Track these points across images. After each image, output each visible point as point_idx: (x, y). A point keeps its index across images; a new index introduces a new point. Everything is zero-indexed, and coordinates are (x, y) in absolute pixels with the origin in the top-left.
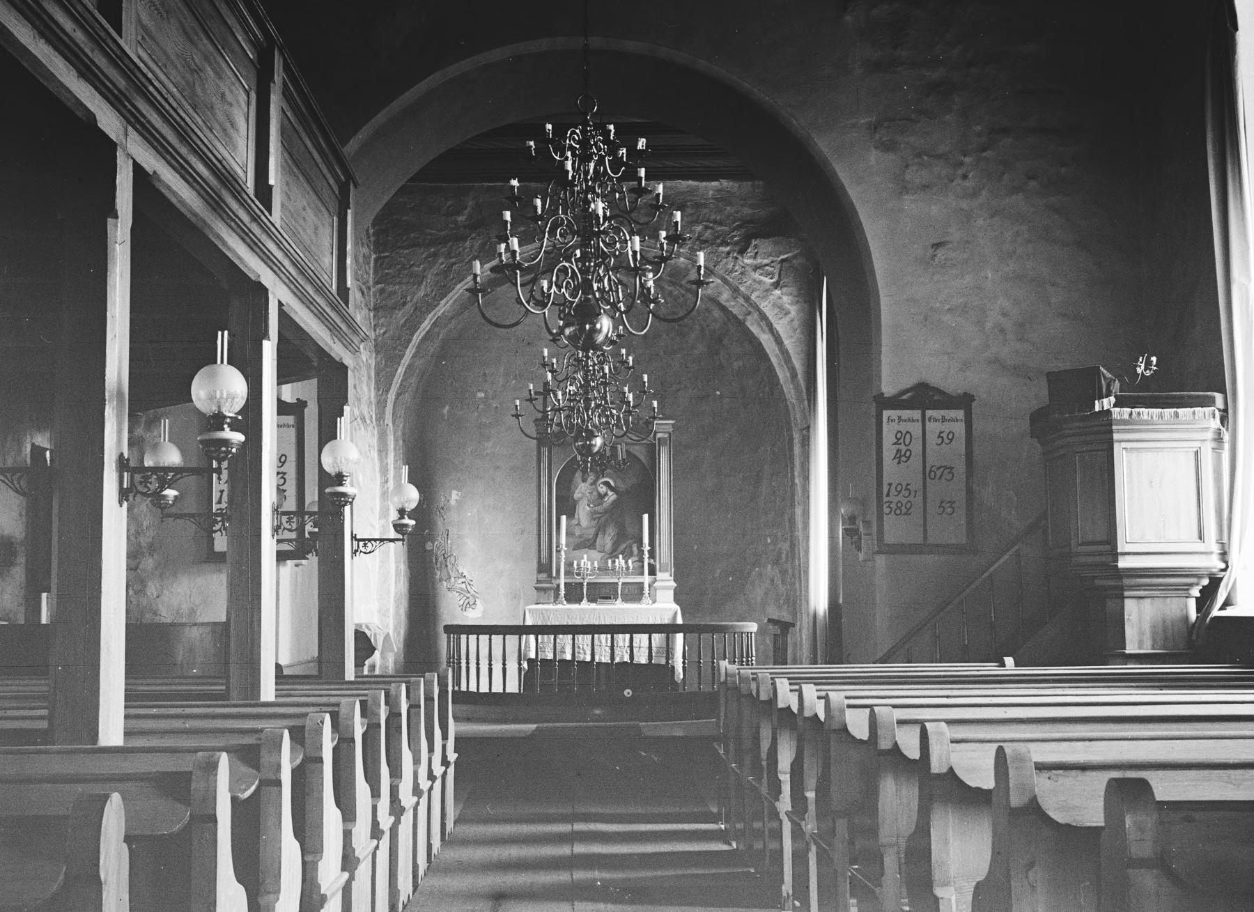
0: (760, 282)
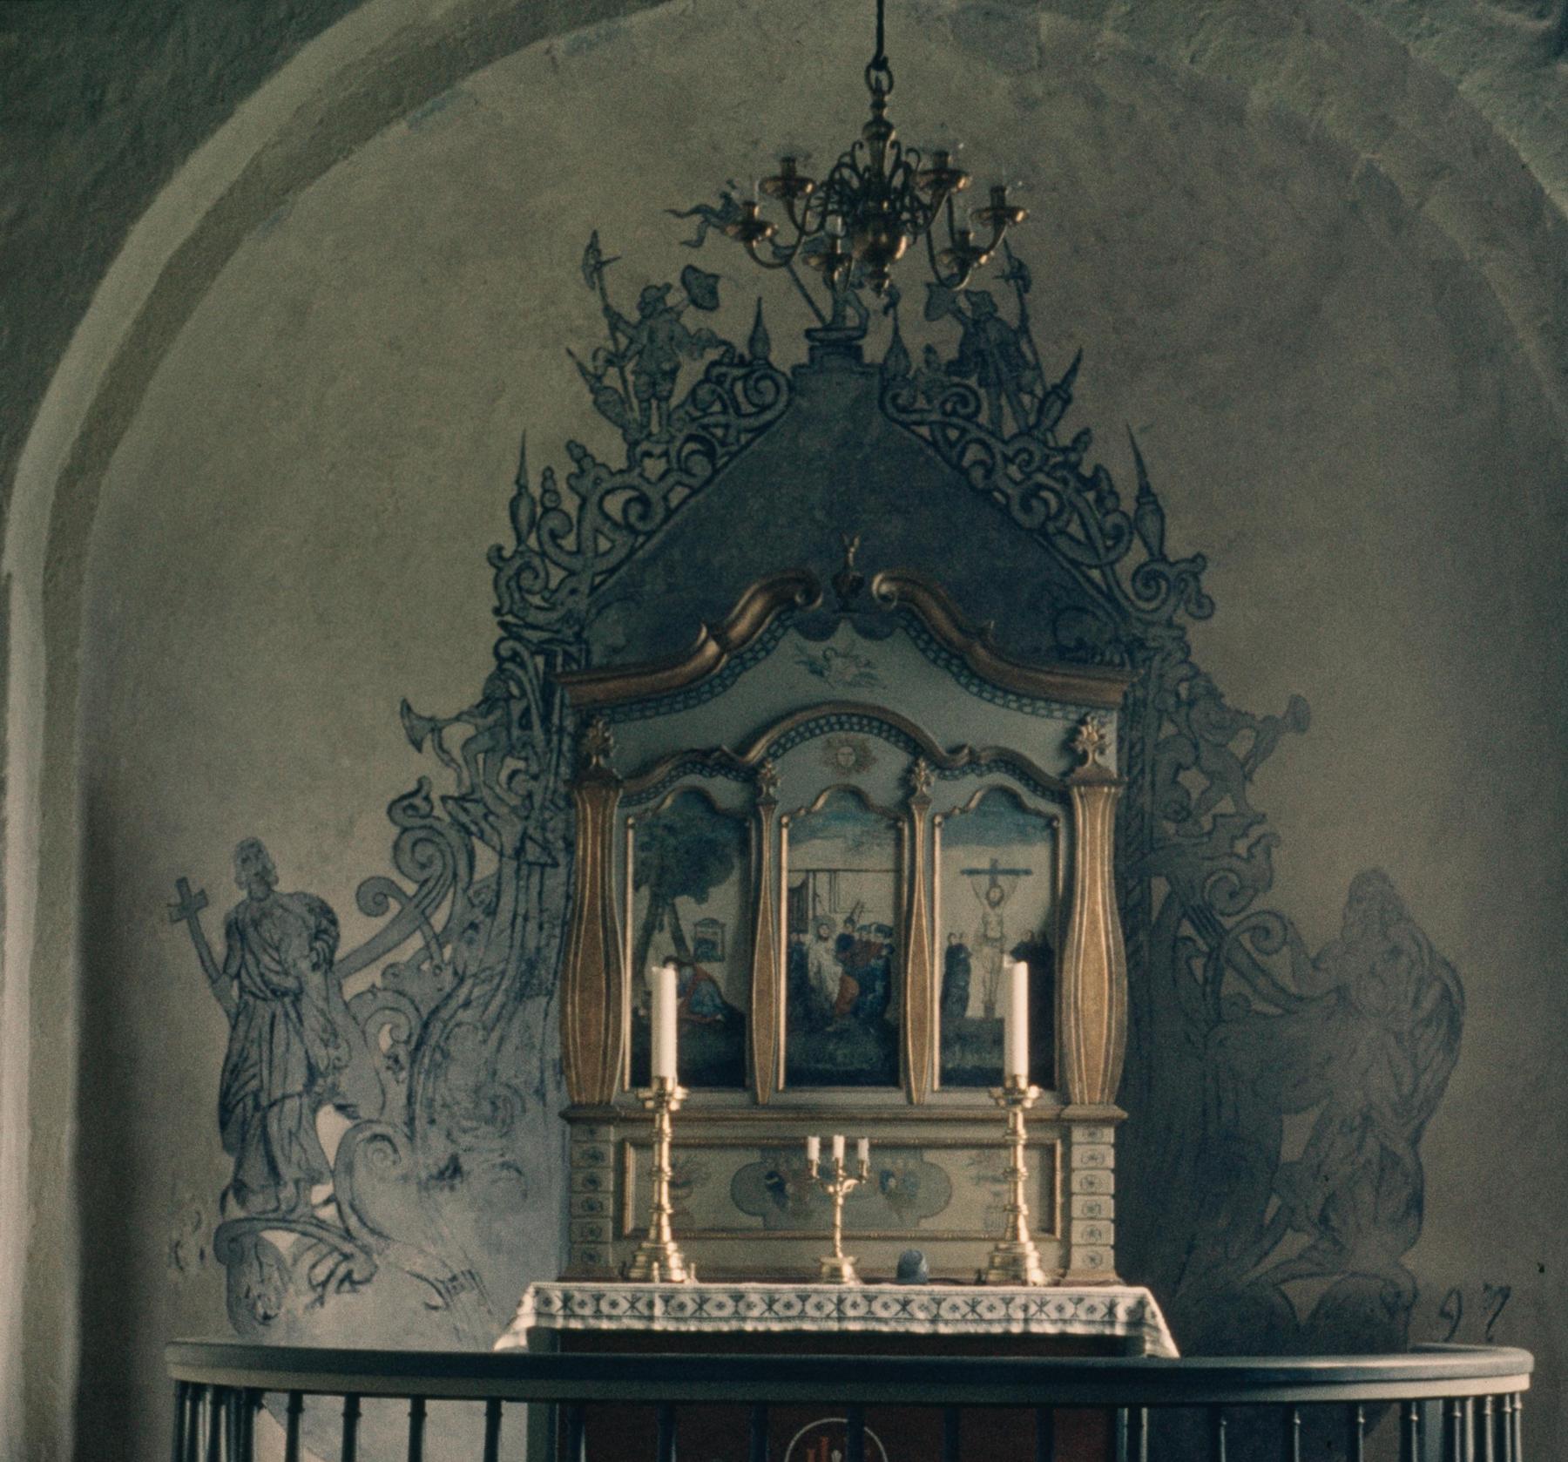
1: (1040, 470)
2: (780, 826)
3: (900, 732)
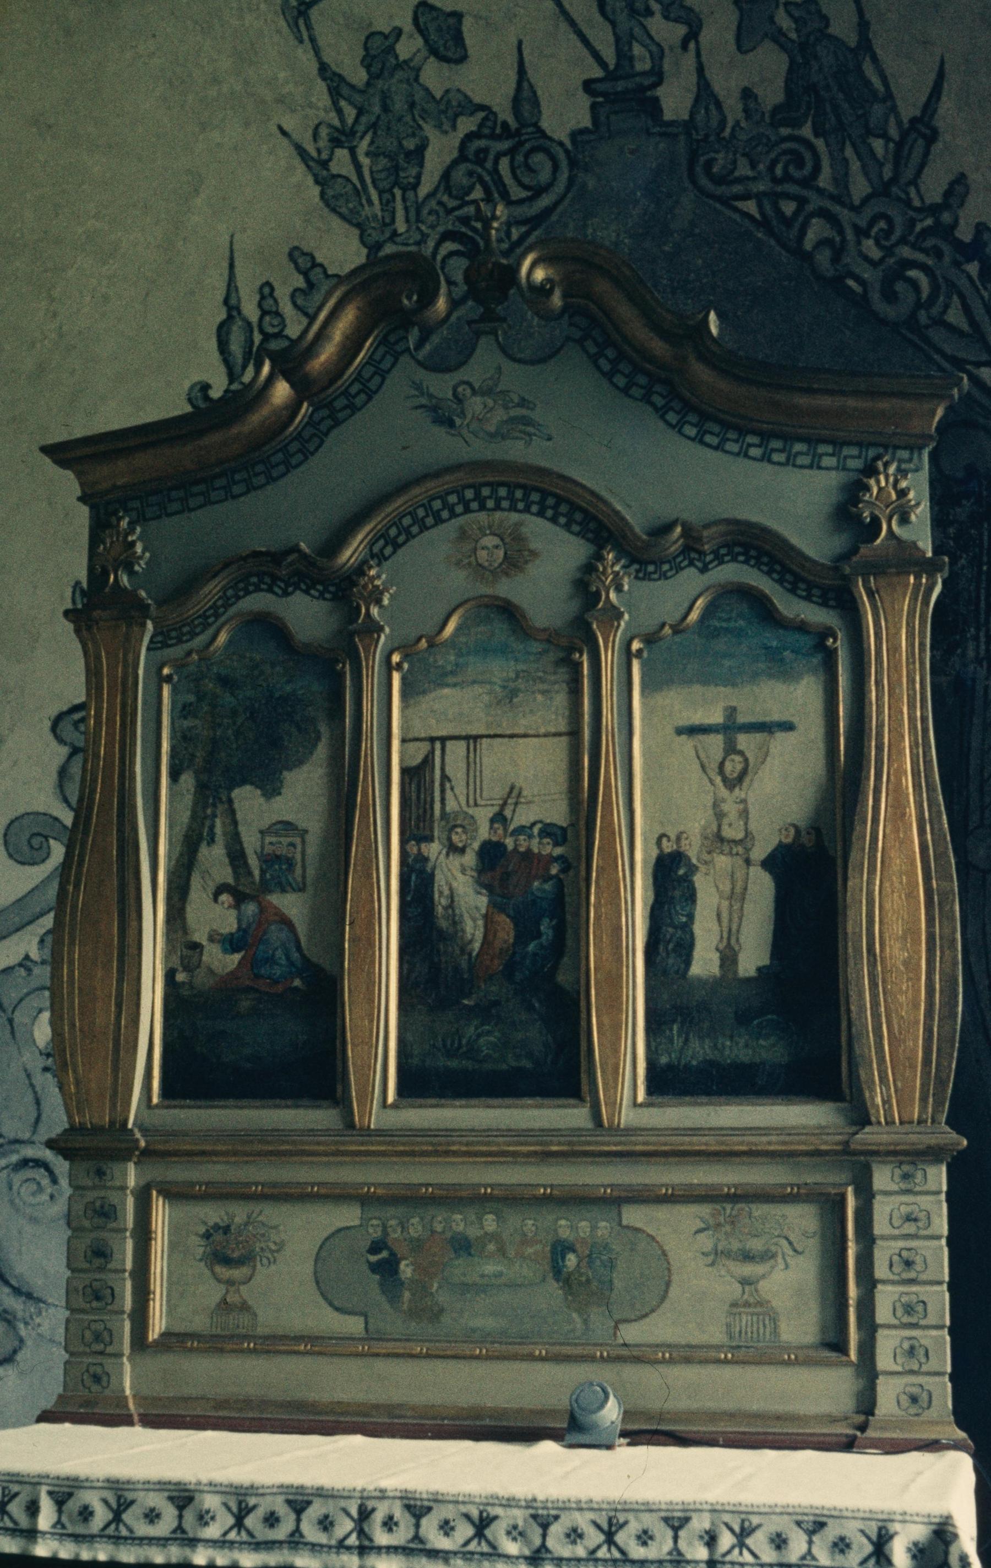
1: (903, 241)
2: (389, 667)
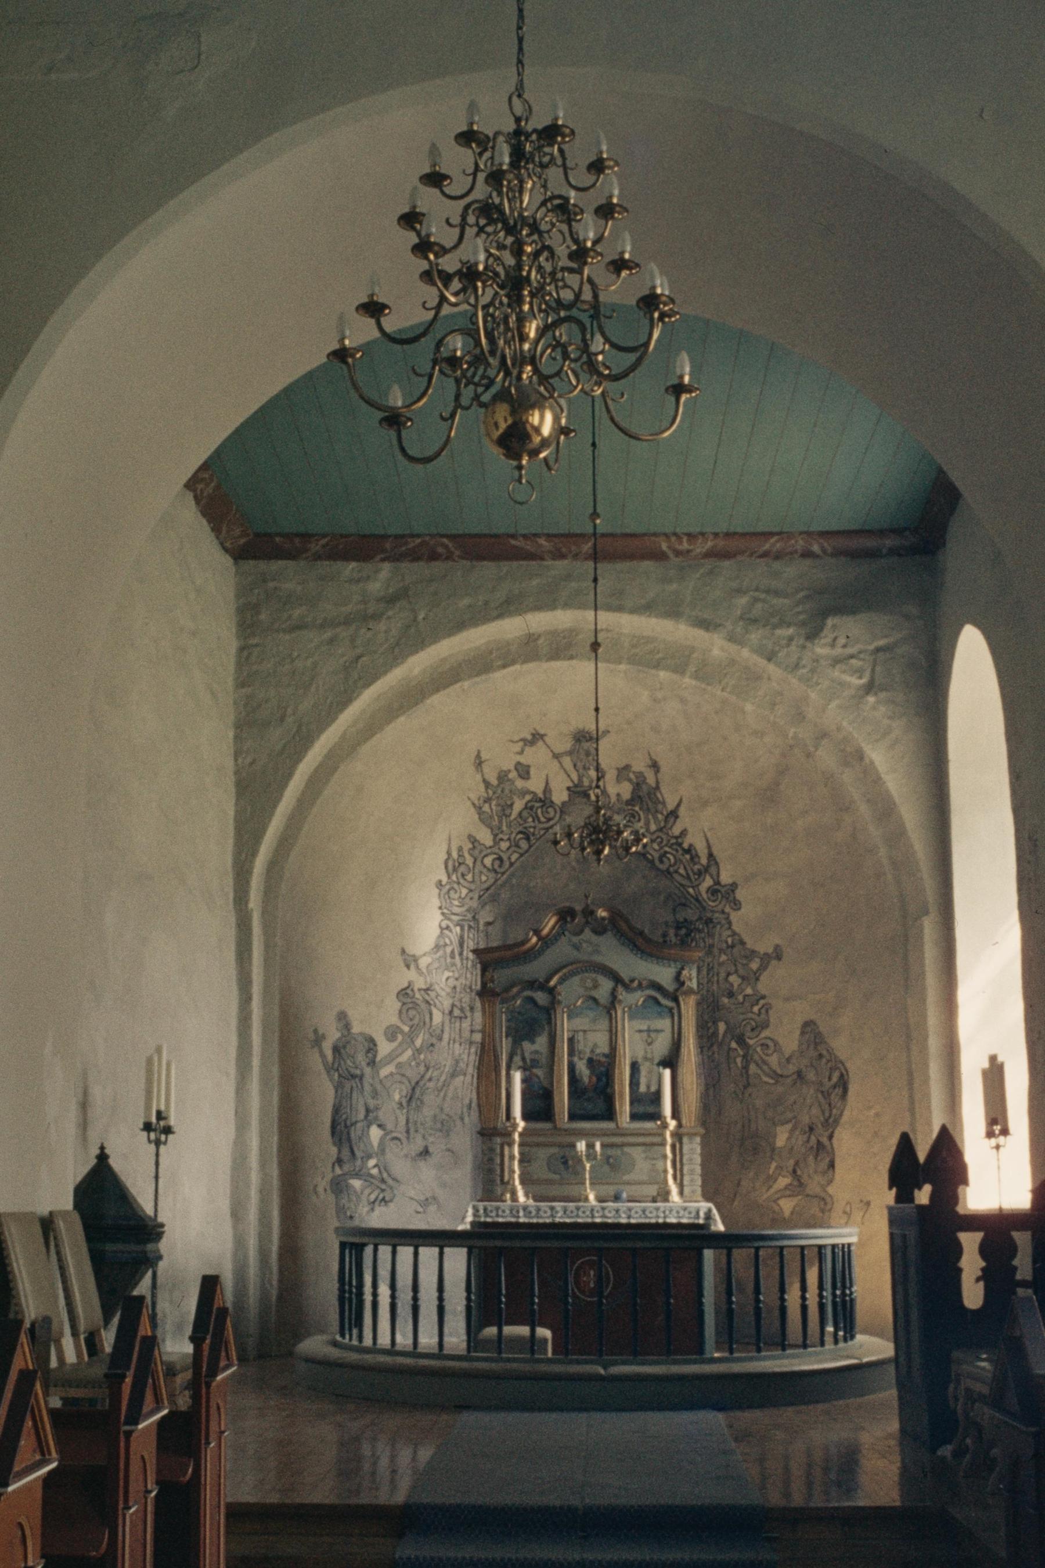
0: (842, 684)
1: (666, 845)
2: (563, 1012)
3: (611, 973)
